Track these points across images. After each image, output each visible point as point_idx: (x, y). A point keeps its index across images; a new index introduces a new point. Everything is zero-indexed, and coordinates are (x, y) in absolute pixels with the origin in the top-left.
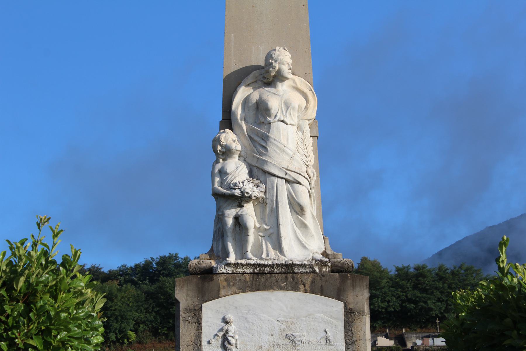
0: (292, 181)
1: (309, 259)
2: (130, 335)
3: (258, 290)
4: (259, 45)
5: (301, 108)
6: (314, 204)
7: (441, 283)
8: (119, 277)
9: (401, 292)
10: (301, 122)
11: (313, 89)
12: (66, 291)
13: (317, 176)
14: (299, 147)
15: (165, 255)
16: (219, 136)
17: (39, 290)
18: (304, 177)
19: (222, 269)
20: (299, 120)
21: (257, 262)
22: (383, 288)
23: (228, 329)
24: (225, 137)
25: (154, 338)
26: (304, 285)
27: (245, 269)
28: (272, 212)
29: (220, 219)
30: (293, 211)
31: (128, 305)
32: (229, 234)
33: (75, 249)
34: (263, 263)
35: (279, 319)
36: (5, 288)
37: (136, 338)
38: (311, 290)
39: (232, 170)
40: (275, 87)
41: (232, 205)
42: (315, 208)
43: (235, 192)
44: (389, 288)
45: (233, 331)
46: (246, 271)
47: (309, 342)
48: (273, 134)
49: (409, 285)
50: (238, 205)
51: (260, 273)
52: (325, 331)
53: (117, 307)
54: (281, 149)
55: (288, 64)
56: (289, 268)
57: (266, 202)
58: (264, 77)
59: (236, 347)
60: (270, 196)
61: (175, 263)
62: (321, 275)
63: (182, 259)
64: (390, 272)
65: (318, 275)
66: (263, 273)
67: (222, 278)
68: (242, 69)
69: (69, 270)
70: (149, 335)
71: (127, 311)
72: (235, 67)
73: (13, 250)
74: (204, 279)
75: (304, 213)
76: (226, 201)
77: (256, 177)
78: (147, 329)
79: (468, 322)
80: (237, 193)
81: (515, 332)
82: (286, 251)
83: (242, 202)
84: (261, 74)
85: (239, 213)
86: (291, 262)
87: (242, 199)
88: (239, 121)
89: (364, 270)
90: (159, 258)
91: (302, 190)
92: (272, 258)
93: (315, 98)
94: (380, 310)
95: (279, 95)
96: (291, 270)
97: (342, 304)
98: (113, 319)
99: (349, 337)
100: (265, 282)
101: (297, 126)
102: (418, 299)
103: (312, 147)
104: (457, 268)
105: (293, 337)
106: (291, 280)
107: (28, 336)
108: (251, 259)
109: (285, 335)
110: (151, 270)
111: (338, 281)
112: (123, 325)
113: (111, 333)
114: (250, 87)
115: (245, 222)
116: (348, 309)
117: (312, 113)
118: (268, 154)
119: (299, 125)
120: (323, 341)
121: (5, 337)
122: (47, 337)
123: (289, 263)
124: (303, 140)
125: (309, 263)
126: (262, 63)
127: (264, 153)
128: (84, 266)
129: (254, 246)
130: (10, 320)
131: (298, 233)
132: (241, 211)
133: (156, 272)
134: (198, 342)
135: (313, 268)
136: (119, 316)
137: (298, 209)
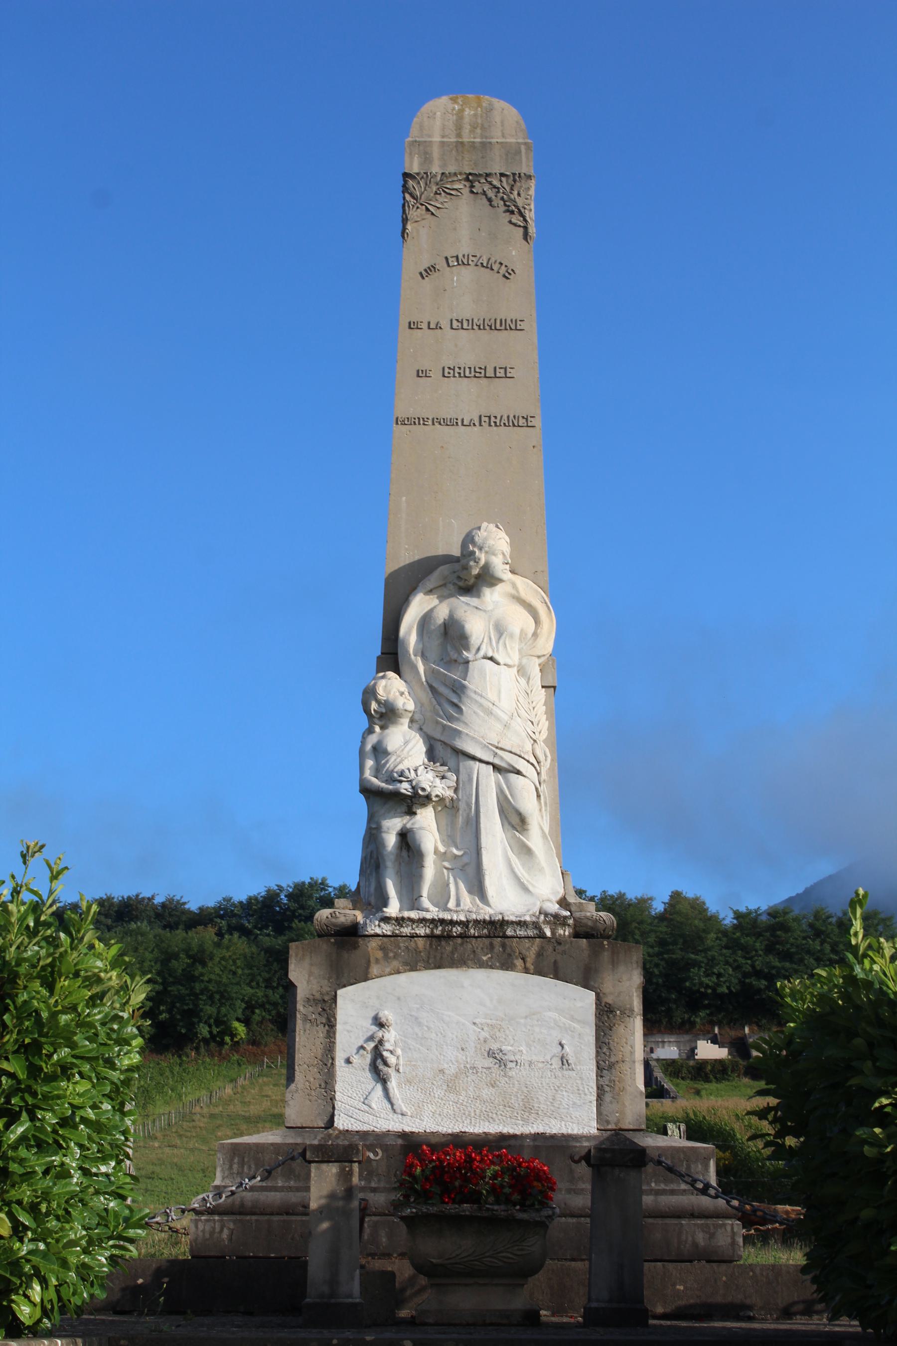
2: (236, 1029)
3: (439, 966)
5: (526, 635)
7: (818, 942)
8: (218, 920)
10: (524, 661)
12: (71, 976)
13: (552, 760)
15: (303, 880)
16: (375, 684)
17: (23, 974)
18: (528, 761)
19: (374, 928)
23: (383, 1037)
24: (386, 686)
25: (280, 1035)
26: (523, 959)
28: (467, 824)
29: (373, 836)
30: (506, 824)
31: (234, 973)
32: (389, 864)
35: (477, 1021)
37: (248, 1034)
38: (535, 968)
39: (397, 746)
40: (478, 596)
43: (400, 788)
44: (721, 950)
45: (392, 1040)
46: (418, 932)
47: (531, 1063)
48: (473, 683)
49: (758, 944)
51: (444, 937)
53: (213, 977)
55: (503, 554)
56: (496, 927)
58: (459, 578)
59: (398, 1071)
61: (321, 897)
63: (334, 888)
64: (724, 919)
66: (449, 937)
67: (373, 944)
68: (419, 562)
69: (77, 938)
70: (272, 1030)
71: (232, 984)
75: (525, 827)
76: (385, 804)
77: (441, 760)
78: (268, 1017)
79: (798, 1040)
81: (869, 1064)
84: (454, 572)
85: (409, 826)
86: (500, 917)
88: (412, 657)
90: (293, 886)
92: (467, 909)
94: (703, 990)
95: (485, 611)
98: (205, 998)
99: (603, 1055)
101: (518, 667)
102: (774, 972)
105: (501, 1054)
108: (427, 910)
109: (487, 1049)
110: (278, 909)
111: (586, 953)
112: (223, 1010)
113: (201, 1025)
116: (603, 1004)
117: (546, 644)
118: (463, 718)
120: (556, 1063)
122: (33, 1057)
125: (534, 919)
126: (456, 552)
128: (153, 897)
133: (288, 913)
134: (328, 1061)
135: (540, 929)
136: (217, 992)
137: (515, 820)
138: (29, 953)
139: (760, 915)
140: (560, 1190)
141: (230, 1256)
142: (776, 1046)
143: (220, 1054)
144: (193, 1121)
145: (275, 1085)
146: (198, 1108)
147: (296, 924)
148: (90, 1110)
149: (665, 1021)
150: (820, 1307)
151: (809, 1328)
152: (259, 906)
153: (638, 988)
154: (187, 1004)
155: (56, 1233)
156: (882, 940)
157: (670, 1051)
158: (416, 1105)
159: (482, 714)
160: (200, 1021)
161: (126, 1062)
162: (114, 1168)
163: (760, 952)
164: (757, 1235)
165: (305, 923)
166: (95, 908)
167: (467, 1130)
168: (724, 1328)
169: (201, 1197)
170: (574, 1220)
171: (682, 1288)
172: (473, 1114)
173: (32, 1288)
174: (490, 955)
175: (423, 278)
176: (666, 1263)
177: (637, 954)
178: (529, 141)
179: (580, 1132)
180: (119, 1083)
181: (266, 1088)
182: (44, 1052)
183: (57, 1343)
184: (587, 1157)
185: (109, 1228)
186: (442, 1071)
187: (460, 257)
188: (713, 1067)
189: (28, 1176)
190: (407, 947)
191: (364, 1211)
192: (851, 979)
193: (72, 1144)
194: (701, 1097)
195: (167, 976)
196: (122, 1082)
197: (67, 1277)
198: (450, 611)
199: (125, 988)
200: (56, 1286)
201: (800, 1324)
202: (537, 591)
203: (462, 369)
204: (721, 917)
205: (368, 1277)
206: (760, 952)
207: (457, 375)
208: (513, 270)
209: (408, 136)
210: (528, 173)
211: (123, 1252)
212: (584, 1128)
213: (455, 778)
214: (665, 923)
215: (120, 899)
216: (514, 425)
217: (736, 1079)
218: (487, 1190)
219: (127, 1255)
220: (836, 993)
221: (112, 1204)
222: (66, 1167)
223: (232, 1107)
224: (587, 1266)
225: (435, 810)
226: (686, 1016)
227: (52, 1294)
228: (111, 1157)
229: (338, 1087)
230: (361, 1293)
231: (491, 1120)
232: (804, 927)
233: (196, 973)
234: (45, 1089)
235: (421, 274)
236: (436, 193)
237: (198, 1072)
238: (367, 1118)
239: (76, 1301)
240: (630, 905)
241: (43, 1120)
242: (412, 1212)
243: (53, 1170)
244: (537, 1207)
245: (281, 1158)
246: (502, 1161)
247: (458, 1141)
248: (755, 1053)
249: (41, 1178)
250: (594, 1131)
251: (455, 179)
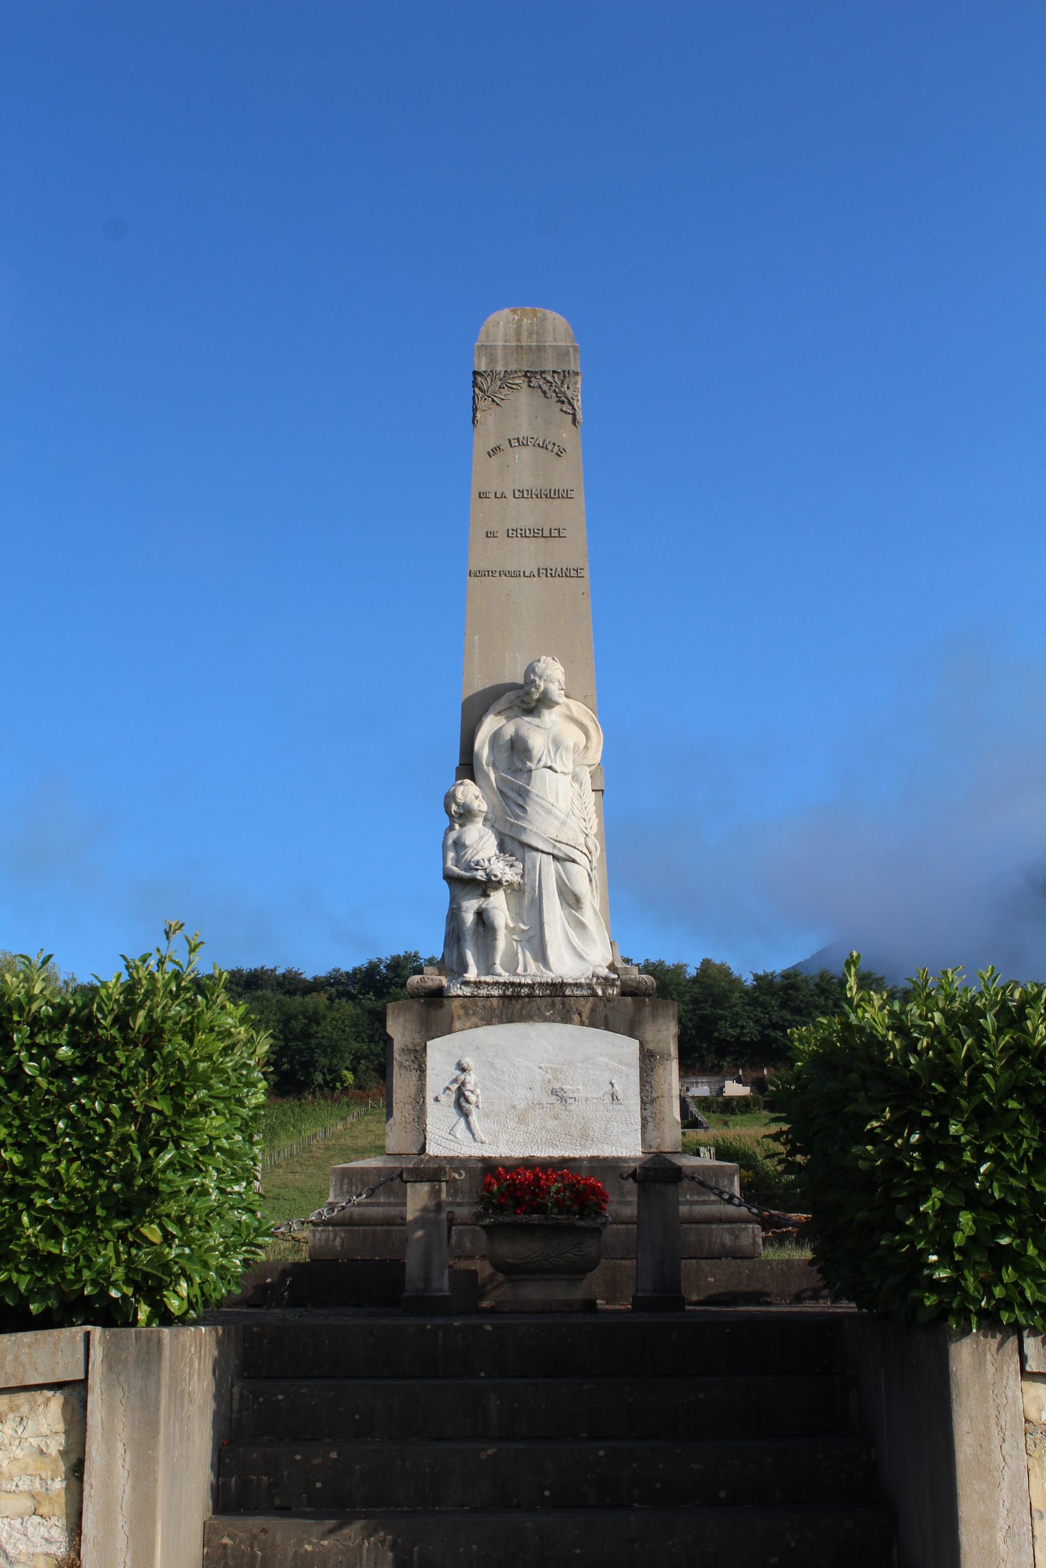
3: (510, 1021)
5: (579, 748)
7: (823, 998)
8: (329, 988)
9: (762, 1012)
10: (577, 769)
12: (207, 1031)
13: (601, 851)
16: (454, 791)
18: (582, 852)
19: (456, 990)
22: (735, 1006)
23: (465, 1079)
24: (463, 791)
26: (580, 1014)
30: (564, 903)
31: (343, 1031)
33: (220, 970)
34: (518, 981)
35: (542, 1065)
36: (117, 1027)
37: (355, 1080)
38: (589, 1021)
40: (539, 716)
46: (492, 993)
47: (587, 1099)
48: (535, 788)
49: (773, 1002)
52: (611, 1083)
53: (325, 1034)
55: (559, 682)
56: (557, 988)
58: (523, 702)
59: (478, 1107)
61: (414, 967)
66: (518, 997)
67: (456, 1003)
69: (211, 1000)
70: (375, 1077)
71: (342, 1039)
73: (131, 970)
74: (429, 1005)
76: (464, 888)
78: (371, 1066)
81: (862, 1094)
84: (519, 697)
85: (484, 906)
86: (560, 980)
88: (485, 767)
89: (706, 979)
95: (544, 729)
97: (636, 1043)
107: (150, 1095)
108: (500, 975)
109: (551, 1088)
112: (335, 1061)
113: (317, 1073)
116: (646, 1050)
117: (595, 755)
118: (528, 817)
120: (608, 1099)
121: (117, 1096)
122: (177, 1097)
123: (557, 981)
125: (588, 981)
126: (520, 680)
130: (125, 1073)
132: (486, 902)
133: (386, 981)
134: (420, 1099)
135: (593, 990)
136: (330, 1046)
137: (572, 900)
138: (173, 1012)
139: (775, 977)
140: (612, 1202)
141: (342, 1260)
142: (787, 1082)
143: (332, 1097)
144: (311, 1152)
145: (378, 1122)
146: (315, 1142)
147: (393, 990)
148: (224, 1141)
149: (698, 1065)
150: (825, 1292)
151: (816, 1310)
152: (363, 975)
153: (674, 1036)
154: (305, 1057)
155: (199, 1240)
156: (872, 993)
157: (702, 1089)
158: (493, 1134)
160: (316, 1070)
161: (254, 1101)
162: (245, 1188)
163: (776, 1008)
164: (775, 1237)
165: (401, 989)
166: (225, 975)
167: (535, 1155)
168: (746, 1311)
169: (317, 1211)
170: (624, 1226)
171: (712, 1280)
172: (540, 1142)
173: (180, 1285)
175: (490, 456)
176: (699, 1260)
177: (673, 1009)
178: (576, 344)
179: (628, 1155)
180: (248, 1119)
181: (371, 1125)
182: (186, 1093)
183: (201, 1330)
184: (633, 1175)
185: (242, 1237)
186: (514, 1107)
187: (521, 439)
188: (738, 1102)
189: (175, 1194)
190: (484, 1006)
191: (451, 1221)
192: (847, 1025)
193: (211, 1168)
194: (728, 1127)
195: (287, 1034)
196: (251, 1118)
197: (209, 1275)
198: (516, 729)
199: (251, 1040)
200: (199, 1284)
201: (808, 1307)
202: (587, 713)
203: (524, 531)
204: (743, 979)
205: (454, 1274)
206: (776, 1008)
207: (519, 535)
208: (564, 449)
209: (477, 341)
210: (575, 371)
211: (254, 1256)
212: (631, 1152)
214: (697, 985)
215: (248, 970)
216: (566, 576)
217: (757, 1111)
218: (552, 1203)
219: (258, 1259)
220: (835, 1037)
221: (244, 1217)
222: (205, 1187)
223: (342, 1140)
224: (635, 1263)
226: (716, 1061)
227: (198, 1293)
228: (243, 1179)
229: (429, 1121)
230: (450, 1288)
231: (555, 1147)
232: (812, 987)
233: (312, 1031)
234: (188, 1123)
235: (488, 453)
236: (500, 387)
237: (314, 1112)
238: (453, 1145)
239: (216, 1295)
240: (668, 971)
241: (186, 1148)
242: (490, 1222)
243: (195, 1189)
244: (593, 1216)
245: (382, 1179)
246: (564, 1179)
247: (528, 1163)
248: (772, 1088)
249: (185, 1196)
250: (639, 1154)
251: (516, 375)
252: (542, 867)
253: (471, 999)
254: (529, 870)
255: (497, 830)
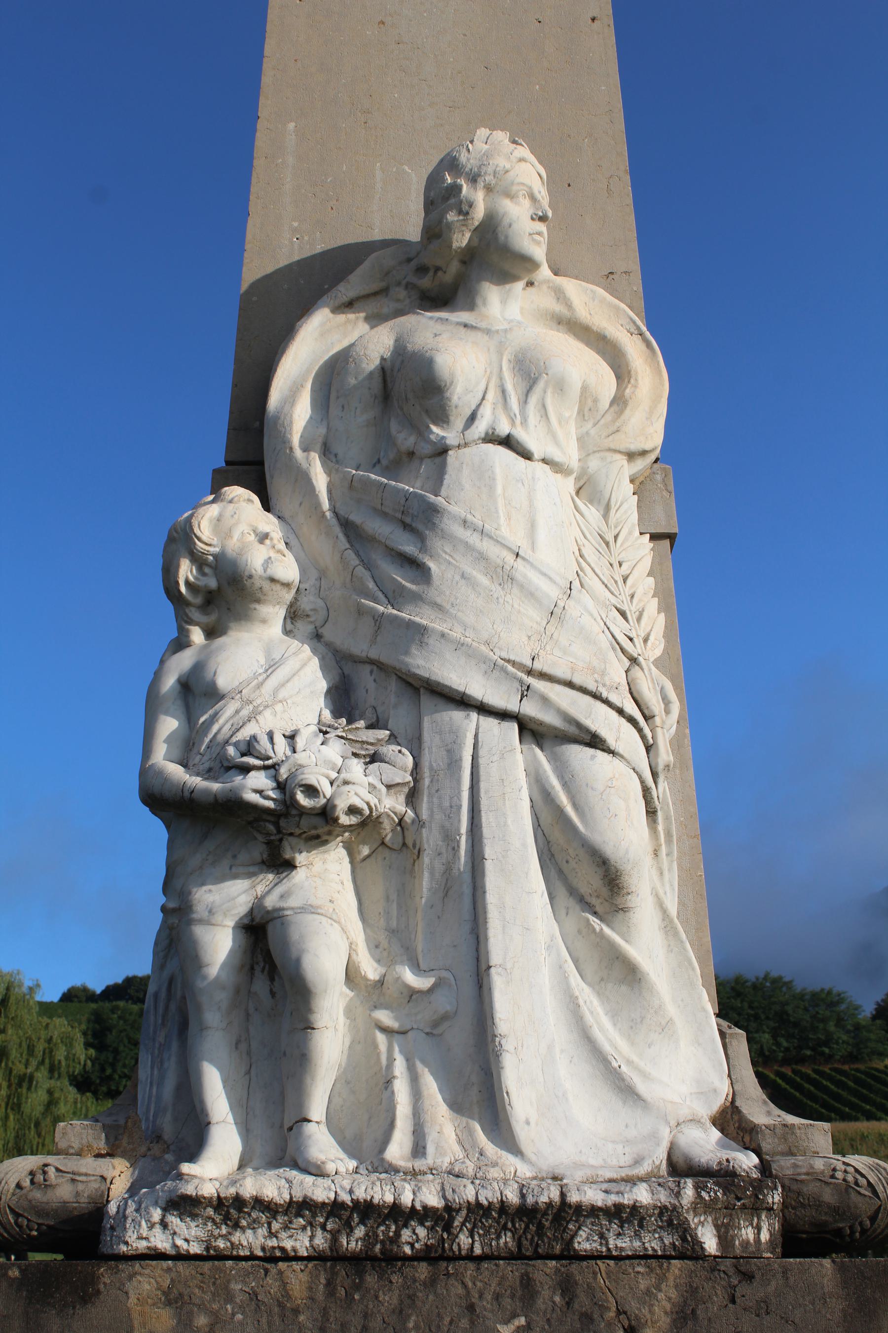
0: (555, 728)
1: (657, 1163)
4: (403, 164)
5: (596, 401)
6: (667, 855)
7: (739, 1001)
10: (594, 464)
11: (644, 329)
14: (584, 564)
16: (189, 520)
18: (620, 712)
20: (589, 455)
21: (351, 1192)
27: (283, 1235)
34: (389, 1198)
39: (244, 673)
41: (234, 857)
42: (673, 876)
43: (243, 787)
46: (288, 1244)
50: (265, 856)
51: (373, 1259)
54: (499, 570)
55: (533, 198)
56: (540, 1226)
57: (414, 846)
60: (435, 810)
62: (731, 1271)
65: (713, 1270)
72: (296, 247)
75: (619, 901)
77: (369, 713)
80: (256, 791)
82: (528, 1123)
83: (285, 843)
84: (409, 260)
85: (270, 902)
86: (554, 1194)
87: (283, 823)
88: (298, 453)
91: (611, 779)
92: (445, 1165)
93: (658, 362)
95: (488, 332)
96: (555, 1239)
100: (401, 1311)
103: (649, 575)
104: (761, 980)
106: (557, 1299)
108: (318, 1171)
111: (837, 1306)
114: (354, 313)
115: (294, 955)
118: (431, 593)
119: (585, 478)
123: (544, 1199)
124: (607, 544)
126: (413, 231)
127: (409, 590)
129: (348, 1082)
131: (592, 1013)
135: (685, 1232)
159: (484, 580)
174: (522, 1321)
213: (409, 761)
225: (351, 854)
252: (482, 761)
253: (207, 1266)
254: (434, 772)
255: (328, 645)
